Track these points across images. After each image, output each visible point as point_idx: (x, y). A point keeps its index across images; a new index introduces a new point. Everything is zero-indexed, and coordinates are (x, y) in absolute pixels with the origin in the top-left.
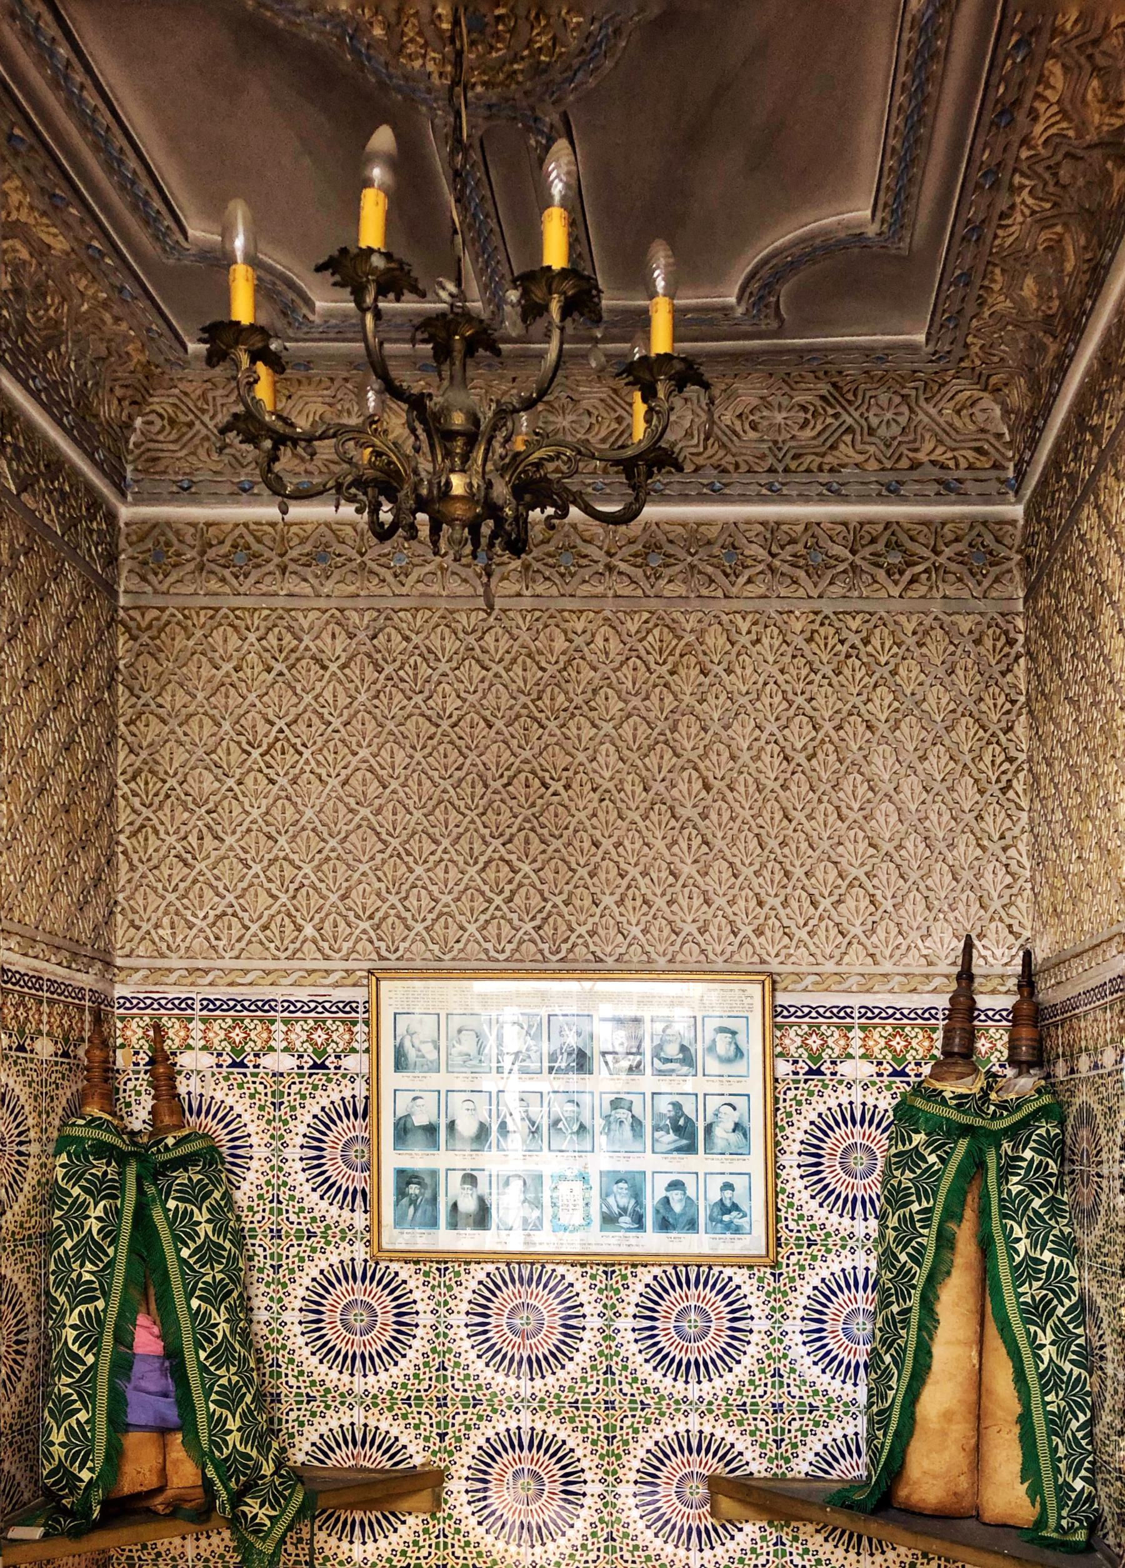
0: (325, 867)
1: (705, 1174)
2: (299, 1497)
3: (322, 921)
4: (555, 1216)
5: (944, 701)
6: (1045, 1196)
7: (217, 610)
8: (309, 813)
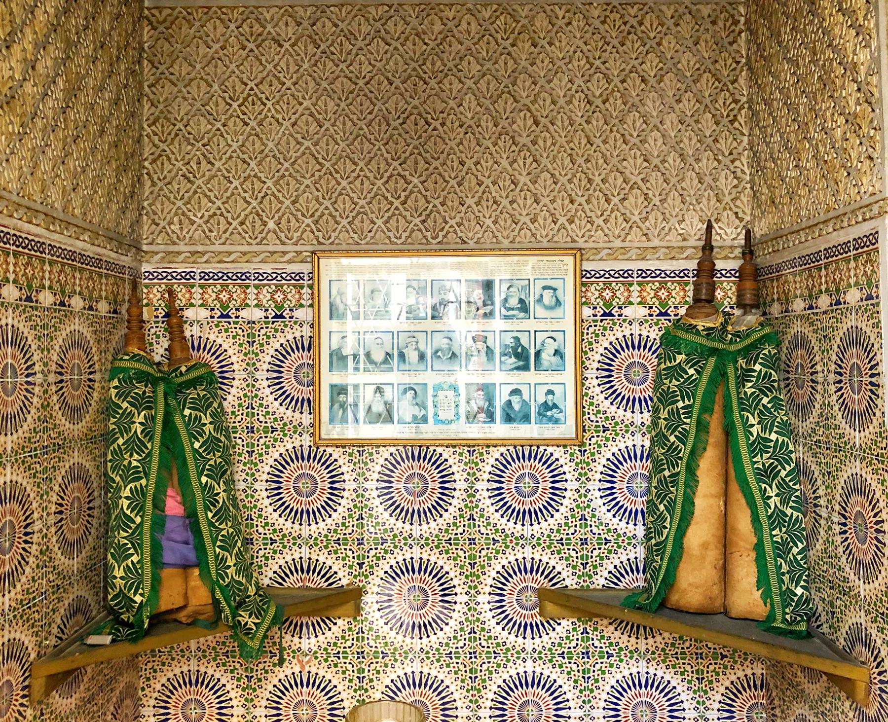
0: (281, 182)
1: (534, 384)
2: (272, 611)
3: (280, 218)
4: (436, 414)
5: (692, 63)
6: (771, 396)
7: (209, 8)
8: (271, 145)
